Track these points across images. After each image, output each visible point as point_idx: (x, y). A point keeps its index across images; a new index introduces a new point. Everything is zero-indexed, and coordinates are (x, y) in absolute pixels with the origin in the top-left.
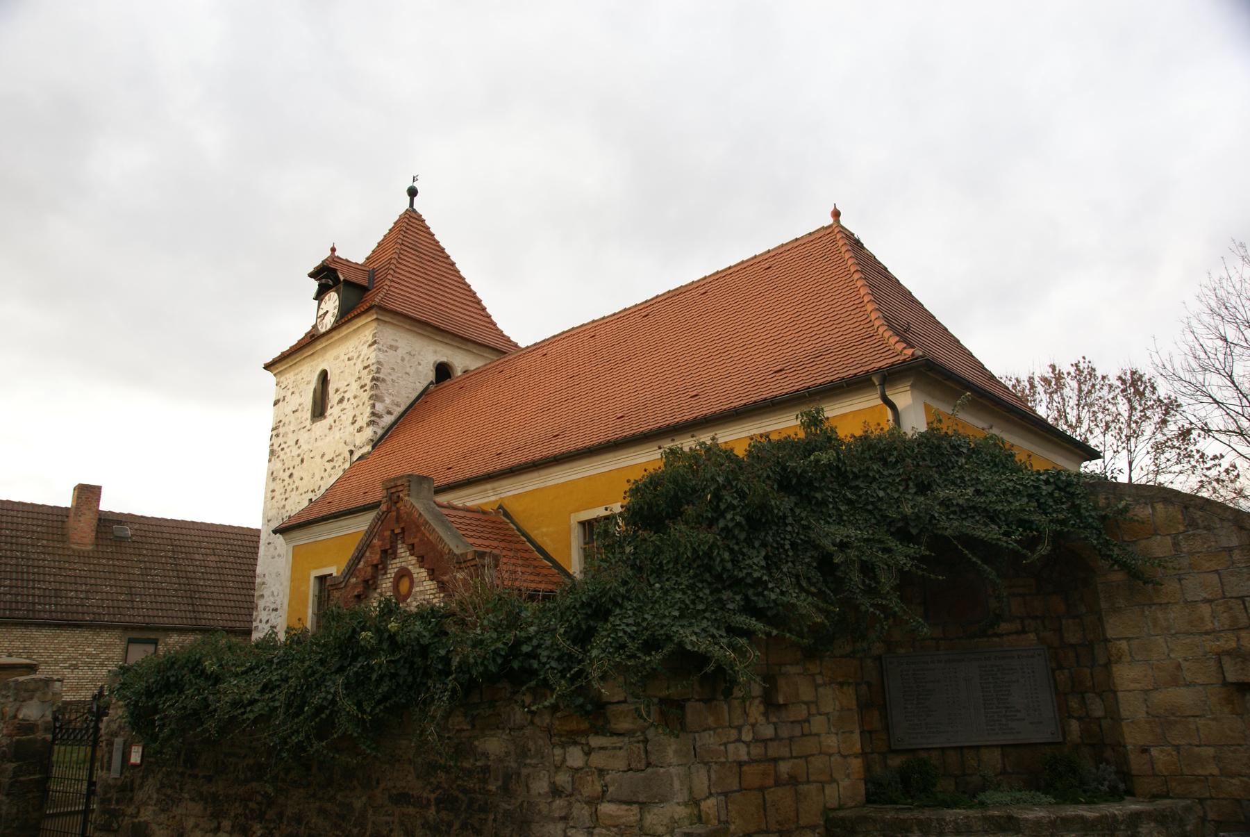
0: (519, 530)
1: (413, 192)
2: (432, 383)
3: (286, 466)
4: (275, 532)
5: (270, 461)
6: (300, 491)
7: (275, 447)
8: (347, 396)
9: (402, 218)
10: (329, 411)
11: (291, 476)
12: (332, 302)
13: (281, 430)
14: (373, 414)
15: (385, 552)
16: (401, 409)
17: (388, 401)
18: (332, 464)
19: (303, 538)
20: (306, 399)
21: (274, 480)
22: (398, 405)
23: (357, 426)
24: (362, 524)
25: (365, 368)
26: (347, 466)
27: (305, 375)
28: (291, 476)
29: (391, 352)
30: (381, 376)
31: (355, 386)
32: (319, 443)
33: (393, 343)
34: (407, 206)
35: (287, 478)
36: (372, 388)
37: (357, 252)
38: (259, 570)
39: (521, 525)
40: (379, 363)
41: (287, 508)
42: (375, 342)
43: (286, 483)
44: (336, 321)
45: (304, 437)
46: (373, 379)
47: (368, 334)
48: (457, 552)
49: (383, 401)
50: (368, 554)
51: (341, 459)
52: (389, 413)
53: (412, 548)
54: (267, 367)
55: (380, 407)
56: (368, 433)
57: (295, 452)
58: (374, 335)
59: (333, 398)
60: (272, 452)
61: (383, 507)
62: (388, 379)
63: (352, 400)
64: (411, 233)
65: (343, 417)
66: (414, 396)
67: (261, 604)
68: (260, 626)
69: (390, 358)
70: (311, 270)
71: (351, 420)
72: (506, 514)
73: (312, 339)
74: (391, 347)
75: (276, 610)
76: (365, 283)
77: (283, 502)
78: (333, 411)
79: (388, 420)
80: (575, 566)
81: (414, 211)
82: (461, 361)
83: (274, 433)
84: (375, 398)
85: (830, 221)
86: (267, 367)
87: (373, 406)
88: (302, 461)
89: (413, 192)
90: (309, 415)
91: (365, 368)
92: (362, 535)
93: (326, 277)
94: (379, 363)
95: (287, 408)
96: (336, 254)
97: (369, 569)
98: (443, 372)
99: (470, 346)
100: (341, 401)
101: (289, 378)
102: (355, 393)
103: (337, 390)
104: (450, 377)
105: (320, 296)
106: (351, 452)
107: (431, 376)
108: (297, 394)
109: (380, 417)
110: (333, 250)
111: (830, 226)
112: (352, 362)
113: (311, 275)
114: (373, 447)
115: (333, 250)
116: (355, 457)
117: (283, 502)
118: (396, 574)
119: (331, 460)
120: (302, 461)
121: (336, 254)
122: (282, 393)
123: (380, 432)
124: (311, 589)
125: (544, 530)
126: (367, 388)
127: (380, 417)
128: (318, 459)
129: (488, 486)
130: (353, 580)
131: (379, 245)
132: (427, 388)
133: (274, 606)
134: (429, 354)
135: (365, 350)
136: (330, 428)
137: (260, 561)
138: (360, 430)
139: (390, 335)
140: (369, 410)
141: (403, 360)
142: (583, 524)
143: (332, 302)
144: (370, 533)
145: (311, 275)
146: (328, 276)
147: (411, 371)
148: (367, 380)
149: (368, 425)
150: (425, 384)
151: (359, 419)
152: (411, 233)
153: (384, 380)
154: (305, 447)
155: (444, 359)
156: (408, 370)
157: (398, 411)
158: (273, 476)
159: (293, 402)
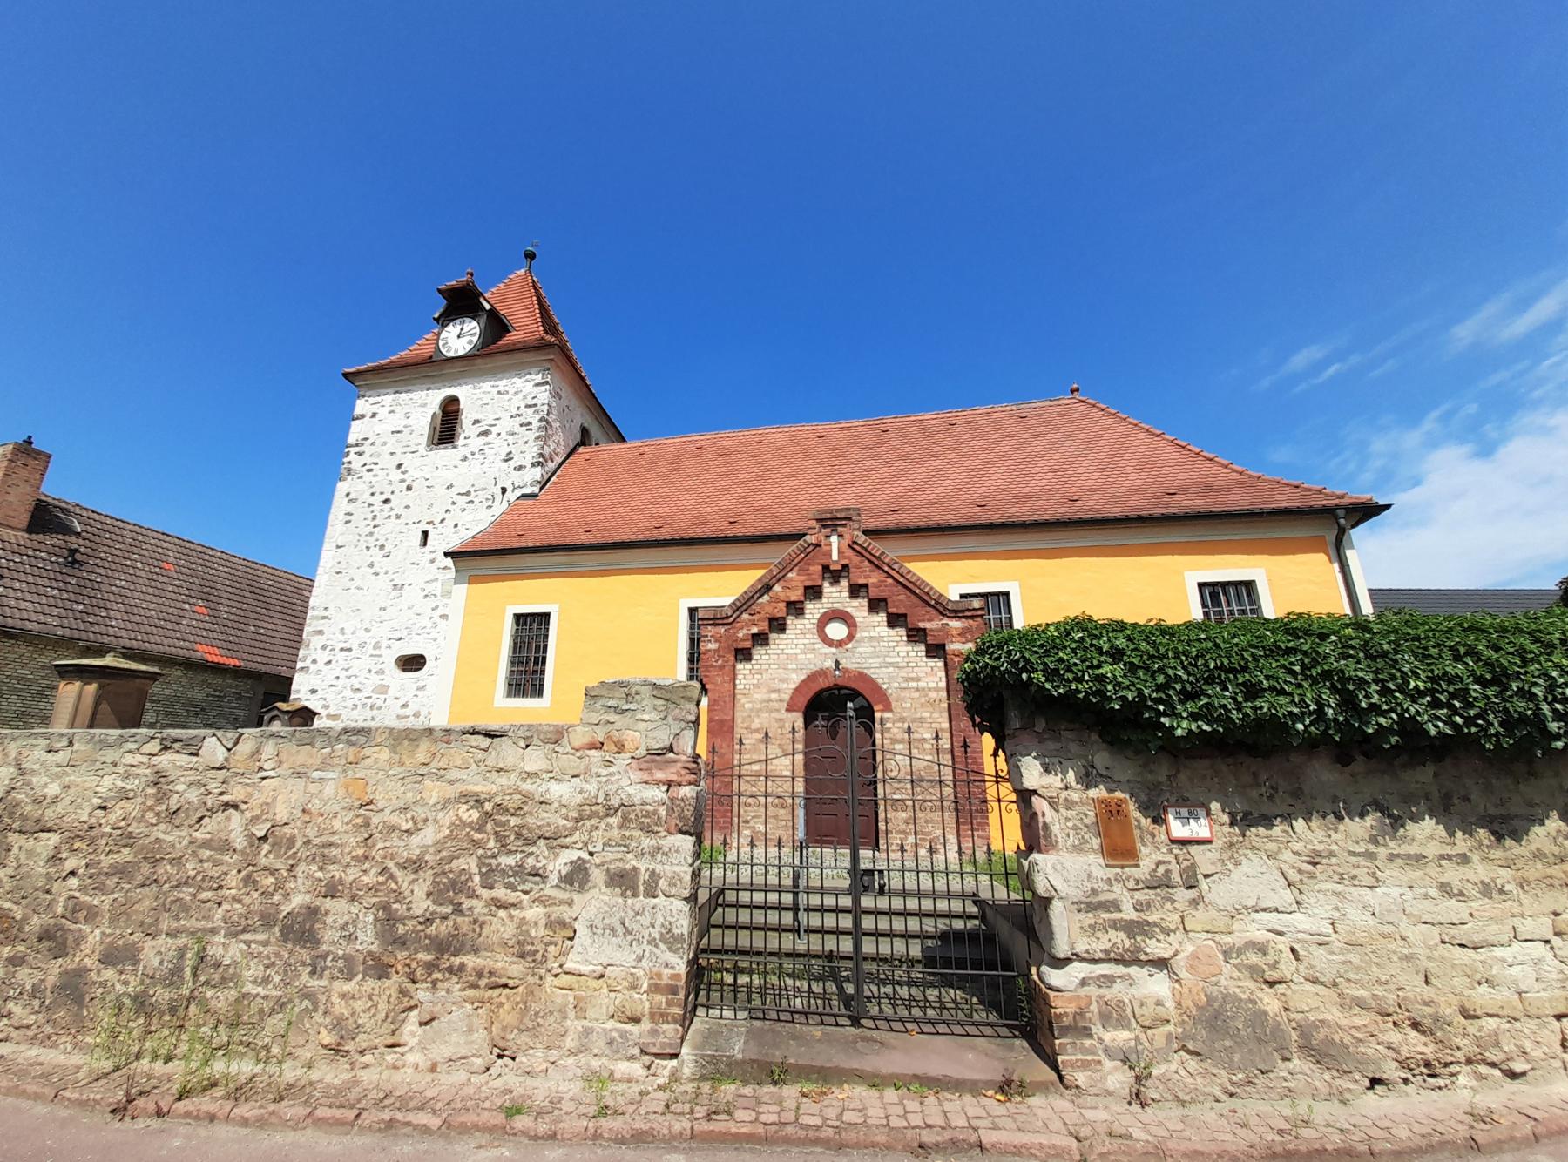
10: (460, 441)
25: (528, 406)
50: (777, 588)
56: (537, 473)
57: (396, 475)
90: (424, 440)
91: (528, 406)
116: (512, 496)
117: (370, 529)
119: (468, 494)
120: (409, 488)
136: (465, 459)
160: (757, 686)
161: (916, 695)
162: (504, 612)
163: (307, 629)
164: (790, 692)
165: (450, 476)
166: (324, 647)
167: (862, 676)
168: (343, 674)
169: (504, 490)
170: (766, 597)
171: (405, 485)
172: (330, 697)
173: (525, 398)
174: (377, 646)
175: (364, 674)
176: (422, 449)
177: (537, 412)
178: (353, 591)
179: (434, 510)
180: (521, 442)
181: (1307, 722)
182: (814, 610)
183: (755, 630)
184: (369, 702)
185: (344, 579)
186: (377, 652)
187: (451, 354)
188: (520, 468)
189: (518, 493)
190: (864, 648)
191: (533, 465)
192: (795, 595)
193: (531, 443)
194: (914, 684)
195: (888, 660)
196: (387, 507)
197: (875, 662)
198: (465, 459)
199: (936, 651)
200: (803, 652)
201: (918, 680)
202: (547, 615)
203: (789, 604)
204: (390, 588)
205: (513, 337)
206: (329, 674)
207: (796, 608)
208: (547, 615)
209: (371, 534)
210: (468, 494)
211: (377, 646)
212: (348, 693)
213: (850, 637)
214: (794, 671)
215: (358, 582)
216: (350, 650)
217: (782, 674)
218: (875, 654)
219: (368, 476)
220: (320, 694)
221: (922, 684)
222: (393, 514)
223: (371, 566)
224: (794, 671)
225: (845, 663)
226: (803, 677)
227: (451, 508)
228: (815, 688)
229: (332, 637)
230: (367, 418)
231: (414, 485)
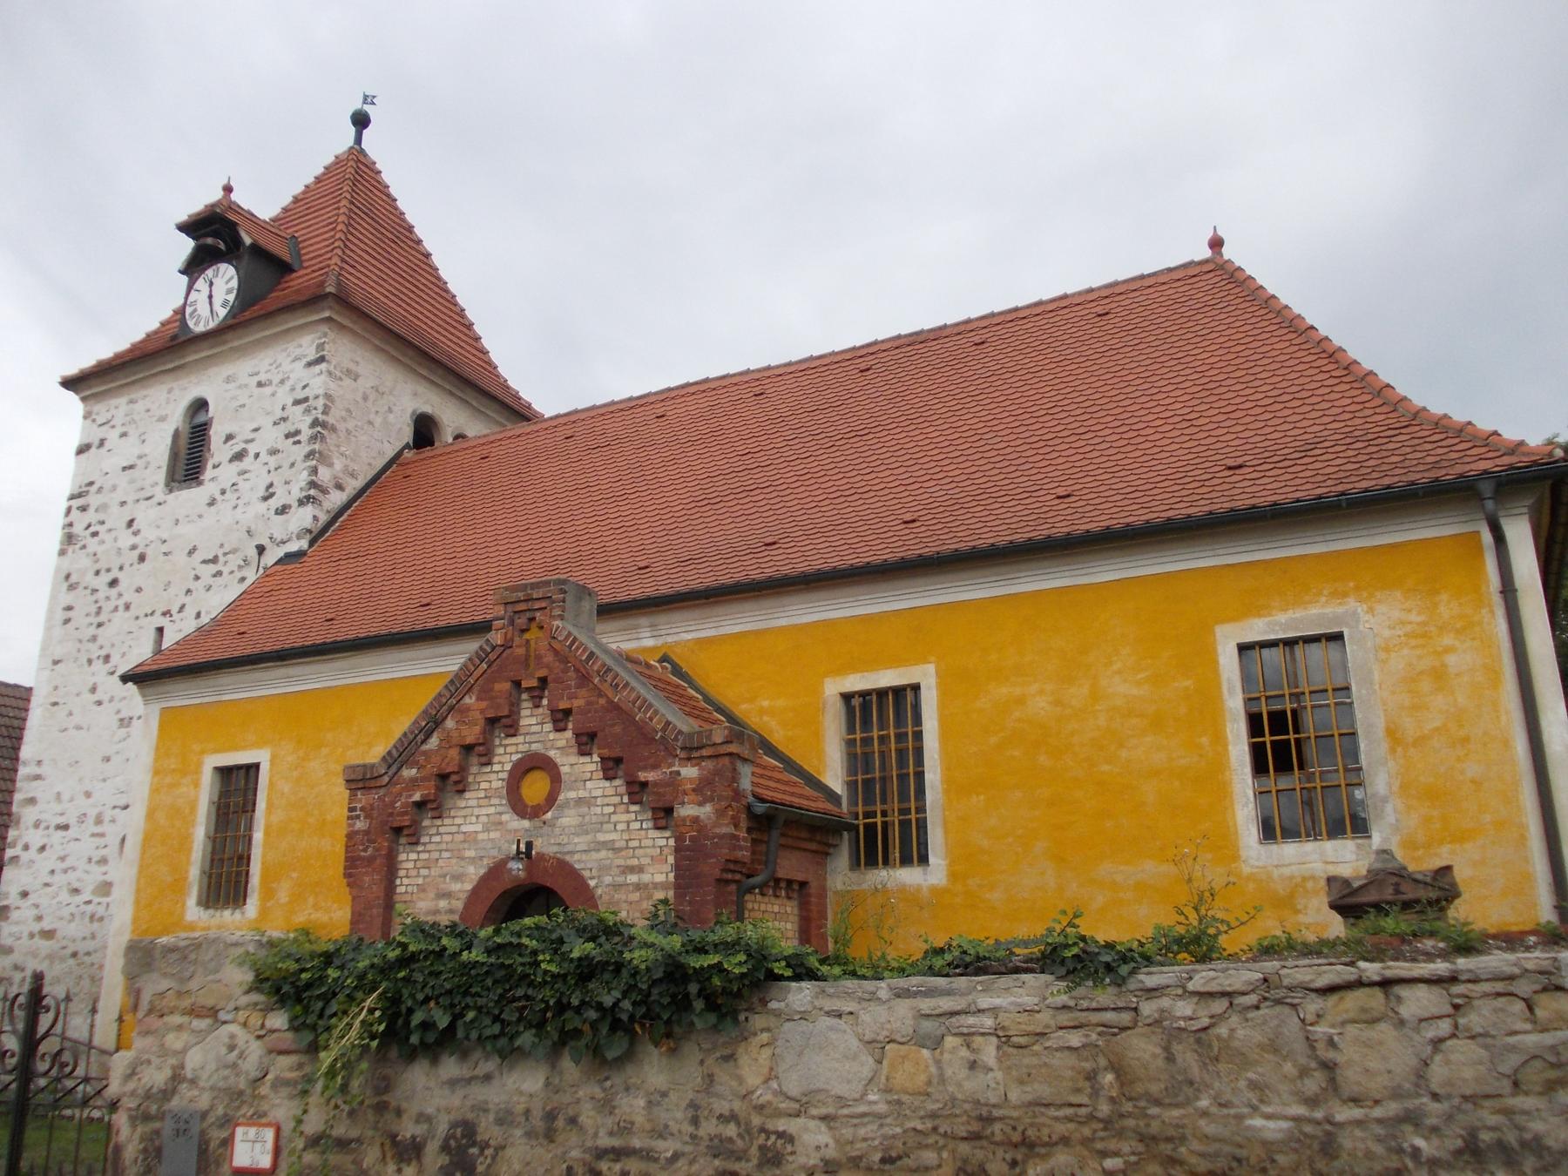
0: (707, 699)
1: (361, 121)
2: (407, 446)
3: (102, 565)
4: (125, 679)
5: (62, 553)
6: (133, 611)
7: (78, 529)
8: (252, 448)
9: (338, 161)
10: (208, 473)
11: (114, 583)
12: (224, 280)
13: (93, 500)
14: (313, 485)
15: (492, 722)
16: (358, 483)
17: (338, 465)
18: (213, 568)
19: (186, 696)
20: (159, 447)
21: (72, 587)
22: (353, 475)
23: (274, 503)
24: (448, 660)
25: (297, 402)
26: (251, 576)
27: (159, 409)
28: (114, 583)
29: (347, 382)
30: (330, 420)
31: (272, 436)
32: (183, 529)
33: (352, 366)
34: (350, 142)
35: (104, 591)
36: (313, 438)
37: (264, 200)
38: (26, 752)
39: (713, 693)
40: (328, 396)
41: (100, 641)
42: (322, 359)
43: (101, 595)
44: (232, 314)
45: (145, 515)
46: (315, 423)
47: (307, 345)
48: (685, 729)
49: (331, 465)
50: (450, 723)
51: (234, 561)
52: (339, 487)
53: (560, 719)
54: (70, 383)
55: (325, 475)
56: (304, 517)
57: (126, 539)
58: (320, 347)
59: (218, 450)
60: (69, 539)
61: (496, 637)
62: (341, 427)
63: (264, 457)
64: (354, 185)
65: (242, 485)
66: (379, 464)
67: (28, 815)
68: (25, 856)
69: (346, 391)
70: (183, 217)
71: (262, 492)
72: (677, 671)
73: (168, 349)
74: (349, 372)
75: (66, 827)
76: (286, 257)
77: (92, 631)
78: (219, 470)
79: (337, 499)
80: (835, 777)
81: (362, 151)
82: (453, 418)
83: (76, 503)
84: (317, 457)
85: (1206, 253)
86: (70, 383)
87: (315, 471)
88: (142, 558)
89: (361, 121)
90: (161, 476)
91: (297, 402)
92: (438, 687)
93: (215, 235)
94: (328, 396)
95: (110, 461)
96: (234, 197)
97: (454, 753)
98: (424, 431)
99: (470, 396)
100: (239, 456)
101: (117, 407)
102: (270, 444)
103: (229, 437)
104: (432, 444)
105: (195, 266)
106: (261, 550)
107: (407, 435)
108: (133, 439)
109: (325, 491)
110: (228, 189)
111: (1206, 261)
112: (267, 390)
113: (188, 228)
114: (312, 543)
115: (228, 189)
116: (271, 558)
117: (92, 631)
118: (517, 765)
119: (214, 560)
120: (142, 558)
121: (234, 197)
122: (96, 434)
123: (324, 518)
124: (205, 792)
125: (766, 703)
126: (303, 437)
127: (325, 491)
128: (180, 558)
129: (644, 621)
130: (409, 773)
131: (296, 200)
132: (399, 454)
133: (61, 820)
134: (407, 397)
135: (298, 372)
136: (212, 503)
137: (29, 736)
138: (283, 510)
139: (346, 351)
140: (304, 477)
141: (365, 398)
142: (847, 697)
143: (224, 280)
144: (458, 684)
145: (188, 228)
146: (215, 234)
147: (378, 421)
148: (303, 423)
149: (301, 503)
150: (399, 445)
151: (279, 490)
152: (354, 185)
153: (334, 429)
154: (149, 534)
155: (427, 409)
156: (372, 416)
157: (352, 486)
158: (69, 582)
159: (125, 451)
160: (422, 889)
161: (635, 896)
162: (200, 765)
163: (18, 797)
164: (464, 896)
165: (190, 532)
166: (37, 825)
167: (564, 868)
168: (60, 866)
169: (261, 550)
170: (434, 742)
171: (136, 553)
172: (44, 902)
173: (293, 389)
174: (99, 821)
175: (82, 865)
176: (159, 492)
177: (308, 411)
178: (72, 732)
179: (172, 590)
180: (286, 465)
181: (7, 1028)
182: (507, 753)
183: (417, 797)
184: (89, 908)
185: (61, 712)
186: (99, 829)
187: (200, 328)
188: (283, 510)
189: (280, 552)
190: (569, 819)
191: (301, 503)
192: (472, 734)
193: (300, 465)
194: (633, 878)
195: (601, 837)
196: (114, 592)
197: (581, 842)
198: (212, 503)
199: (663, 815)
200: (487, 830)
201: (640, 869)
202: (257, 766)
203: (468, 749)
204: (116, 724)
205: (299, 281)
206: (47, 862)
207: (478, 751)
208: (257, 766)
209: (94, 639)
210: (214, 560)
211: (99, 821)
212: (64, 896)
213: (551, 800)
214: (472, 860)
215: (76, 719)
216: (66, 827)
217: (455, 866)
218: (582, 829)
219: (93, 544)
220: (32, 899)
221: (646, 878)
222: (121, 602)
223: (93, 690)
224: (472, 860)
225: (539, 846)
226: (482, 871)
227: (192, 585)
228: (499, 888)
229: (46, 810)
230: (93, 449)
231: (149, 552)
